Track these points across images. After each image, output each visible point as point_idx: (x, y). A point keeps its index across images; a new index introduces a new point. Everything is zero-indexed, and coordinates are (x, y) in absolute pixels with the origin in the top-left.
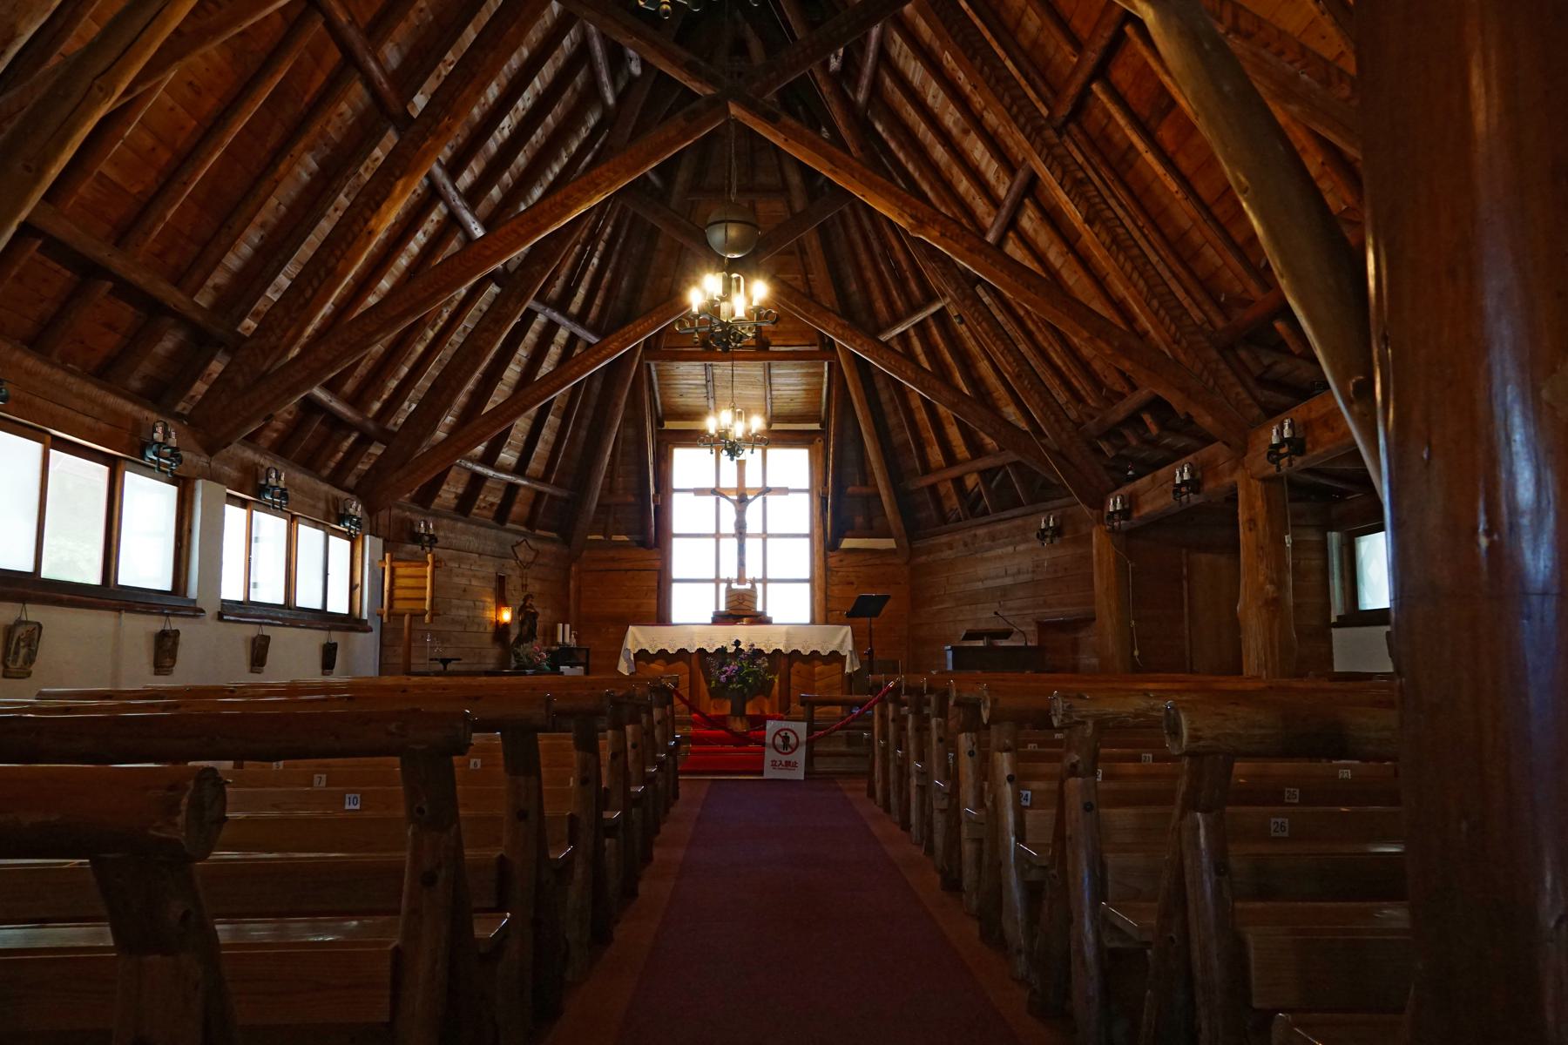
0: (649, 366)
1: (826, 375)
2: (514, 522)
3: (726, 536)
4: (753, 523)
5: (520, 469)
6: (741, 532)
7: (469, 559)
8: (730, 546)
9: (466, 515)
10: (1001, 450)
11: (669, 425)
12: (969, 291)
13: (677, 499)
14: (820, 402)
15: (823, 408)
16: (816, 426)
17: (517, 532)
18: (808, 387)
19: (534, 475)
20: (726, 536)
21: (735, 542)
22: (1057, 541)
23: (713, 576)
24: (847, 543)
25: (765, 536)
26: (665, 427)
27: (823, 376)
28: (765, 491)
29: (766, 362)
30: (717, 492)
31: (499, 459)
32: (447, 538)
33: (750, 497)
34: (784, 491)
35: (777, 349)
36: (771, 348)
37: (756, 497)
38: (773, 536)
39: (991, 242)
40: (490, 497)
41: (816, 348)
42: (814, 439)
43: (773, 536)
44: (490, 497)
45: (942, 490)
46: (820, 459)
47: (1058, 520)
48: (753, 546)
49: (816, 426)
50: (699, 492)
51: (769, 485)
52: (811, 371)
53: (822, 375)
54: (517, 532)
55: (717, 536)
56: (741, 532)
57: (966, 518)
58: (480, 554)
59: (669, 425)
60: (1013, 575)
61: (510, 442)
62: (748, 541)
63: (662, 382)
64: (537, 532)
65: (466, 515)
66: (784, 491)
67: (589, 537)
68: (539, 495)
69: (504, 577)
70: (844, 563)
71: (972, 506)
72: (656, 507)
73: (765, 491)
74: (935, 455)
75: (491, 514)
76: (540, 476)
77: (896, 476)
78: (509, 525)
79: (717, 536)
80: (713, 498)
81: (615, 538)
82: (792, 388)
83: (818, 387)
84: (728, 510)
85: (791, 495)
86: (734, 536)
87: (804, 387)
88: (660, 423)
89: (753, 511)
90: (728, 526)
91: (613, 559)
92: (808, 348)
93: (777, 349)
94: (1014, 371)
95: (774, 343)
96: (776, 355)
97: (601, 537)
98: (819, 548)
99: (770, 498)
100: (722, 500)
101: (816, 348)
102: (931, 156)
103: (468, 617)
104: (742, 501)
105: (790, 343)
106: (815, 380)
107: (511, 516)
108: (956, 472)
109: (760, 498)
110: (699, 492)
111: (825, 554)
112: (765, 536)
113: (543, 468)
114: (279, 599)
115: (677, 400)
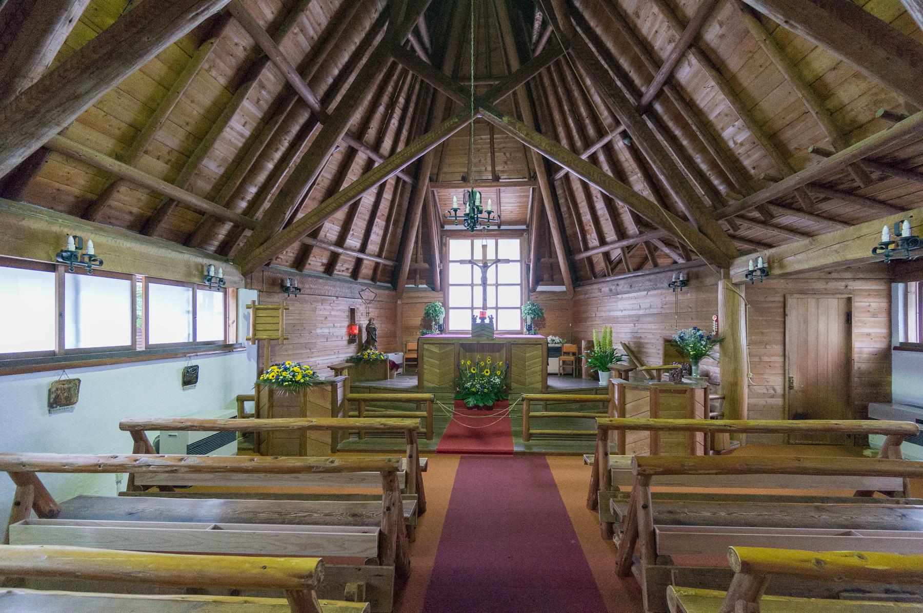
0: (433, 192)
1: (531, 196)
2: (364, 278)
3: (477, 285)
4: (491, 279)
5: (363, 249)
6: (484, 283)
7: (327, 300)
8: (479, 290)
9: (330, 275)
10: (641, 233)
11: (447, 227)
12: (638, 119)
13: (452, 266)
14: (527, 213)
15: (528, 216)
16: (524, 227)
17: (364, 284)
18: (520, 204)
19: (372, 253)
20: (477, 285)
21: (481, 288)
22: (685, 289)
23: (499, 287)
24: (540, 288)
25: (497, 285)
26: (445, 229)
27: (529, 197)
28: (497, 261)
29: (498, 188)
30: (472, 262)
31: (346, 243)
32: (311, 288)
33: (489, 265)
34: (507, 261)
35: (504, 180)
36: (500, 180)
37: (492, 265)
38: (501, 285)
39: (417, 379)
40: (366, 270)
41: (526, 180)
42: (523, 234)
43: (501, 285)
44: (366, 270)
45: (595, 260)
46: (526, 245)
47: (685, 276)
48: (491, 290)
49: (524, 227)
50: (462, 262)
51: (499, 258)
52: (523, 194)
53: (528, 197)
54: (364, 284)
55: (472, 285)
56: (484, 283)
57: (609, 275)
58: (337, 297)
59: (447, 227)
60: (646, 309)
61: (353, 234)
62: (488, 287)
63: (441, 203)
64: (378, 283)
65: (330, 275)
66: (507, 261)
67: (406, 286)
68: (377, 264)
69: (354, 309)
70: (539, 298)
71: (613, 266)
72: (441, 271)
73: (497, 261)
74: (593, 239)
75: (349, 274)
76: (376, 254)
77: (569, 252)
78: (360, 280)
79: (472, 285)
80: (470, 265)
81: (420, 286)
82: (511, 205)
83: (526, 204)
84: (478, 271)
85: (511, 263)
86: (481, 285)
87: (518, 204)
88: (442, 226)
89: (491, 271)
90: (478, 280)
91: (418, 297)
92: (521, 180)
93: (504, 180)
94: (669, 174)
95: (502, 178)
96: (504, 184)
97: (414, 286)
98: (525, 291)
99: (499, 265)
100: (475, 266)
101: (526, 180)
102: (621, 7)
103: (329, 333)
104: (485, 267)
105: (511, 177)
106: (525, 199)
107: (361, 275)
108: (605, 249)
109: (494, 265)
110: (462, 262)
111: (528, 294)
112: (497, 285)
113: (378, 250)
114: (450, 306)
115: (379, 4)
